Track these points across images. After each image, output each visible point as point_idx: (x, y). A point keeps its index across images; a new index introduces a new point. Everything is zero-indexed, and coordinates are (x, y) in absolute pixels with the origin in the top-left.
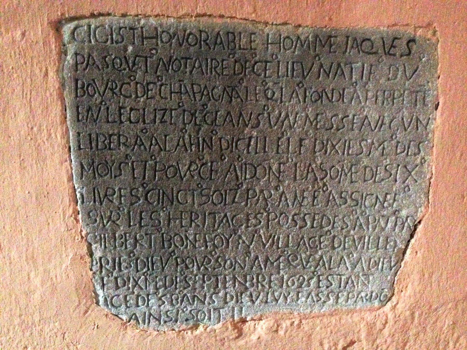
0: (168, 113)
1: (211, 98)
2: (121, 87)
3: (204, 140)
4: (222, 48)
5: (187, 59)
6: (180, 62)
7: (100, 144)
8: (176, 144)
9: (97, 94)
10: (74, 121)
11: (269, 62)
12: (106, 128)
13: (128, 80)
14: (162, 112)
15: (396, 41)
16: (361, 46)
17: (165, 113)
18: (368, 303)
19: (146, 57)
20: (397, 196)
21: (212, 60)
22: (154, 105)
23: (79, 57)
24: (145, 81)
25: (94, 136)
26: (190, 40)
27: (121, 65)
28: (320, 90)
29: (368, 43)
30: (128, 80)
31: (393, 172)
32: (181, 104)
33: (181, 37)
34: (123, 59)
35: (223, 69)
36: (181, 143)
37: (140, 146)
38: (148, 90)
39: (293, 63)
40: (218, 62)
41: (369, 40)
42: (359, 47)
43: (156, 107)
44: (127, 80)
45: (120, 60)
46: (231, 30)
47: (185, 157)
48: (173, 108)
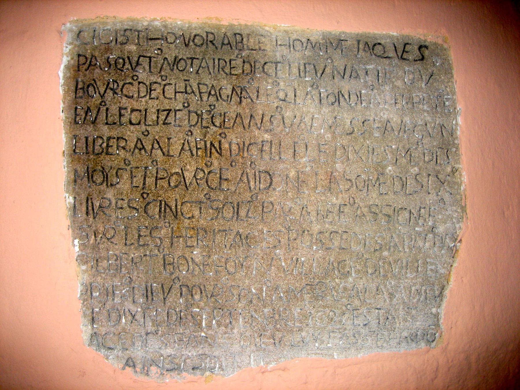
0: (172, 114)
1: (219, 98)
2: (123, 86)
3: (211, 144)
4: (230, 48)
5: (192, 59)
6: (186, 63)
7: (96, 148)
8: (180, 148)
9: (355, 188)
10: (71, 123)
11: (280, 62)
12: (106, 131)
13: (131, 81)
14: (166, 113)
15: (407, 46)
16: (373, 49)
17: (168, 114)
18: (414, 345)
19: (150, 58)
20: (440, 176)
21: (219, 60)
22: (157, 105)
23: (81, 58)
24: (148, 81)
25: (90, 139)
26: (196, 41)
27: (124, 65)
28: (336, 91)
29: (380, 48)
30: (131, 81)
31: (425, 184)
32: (186, 105)
33: (188, 40)
34: (126, 59)
35: (231, 68)
36: (186, 147)
37: (140, 150)
38: (151, 90)
39: (305, 64)
40: (226, 62)
41: (379, 44)
42: (371, 51)
43: (159, 107)
44: (129, 80)
45: (124, 60)
46: (238, 32)
47: (190, 163)
48: (177, 108)
